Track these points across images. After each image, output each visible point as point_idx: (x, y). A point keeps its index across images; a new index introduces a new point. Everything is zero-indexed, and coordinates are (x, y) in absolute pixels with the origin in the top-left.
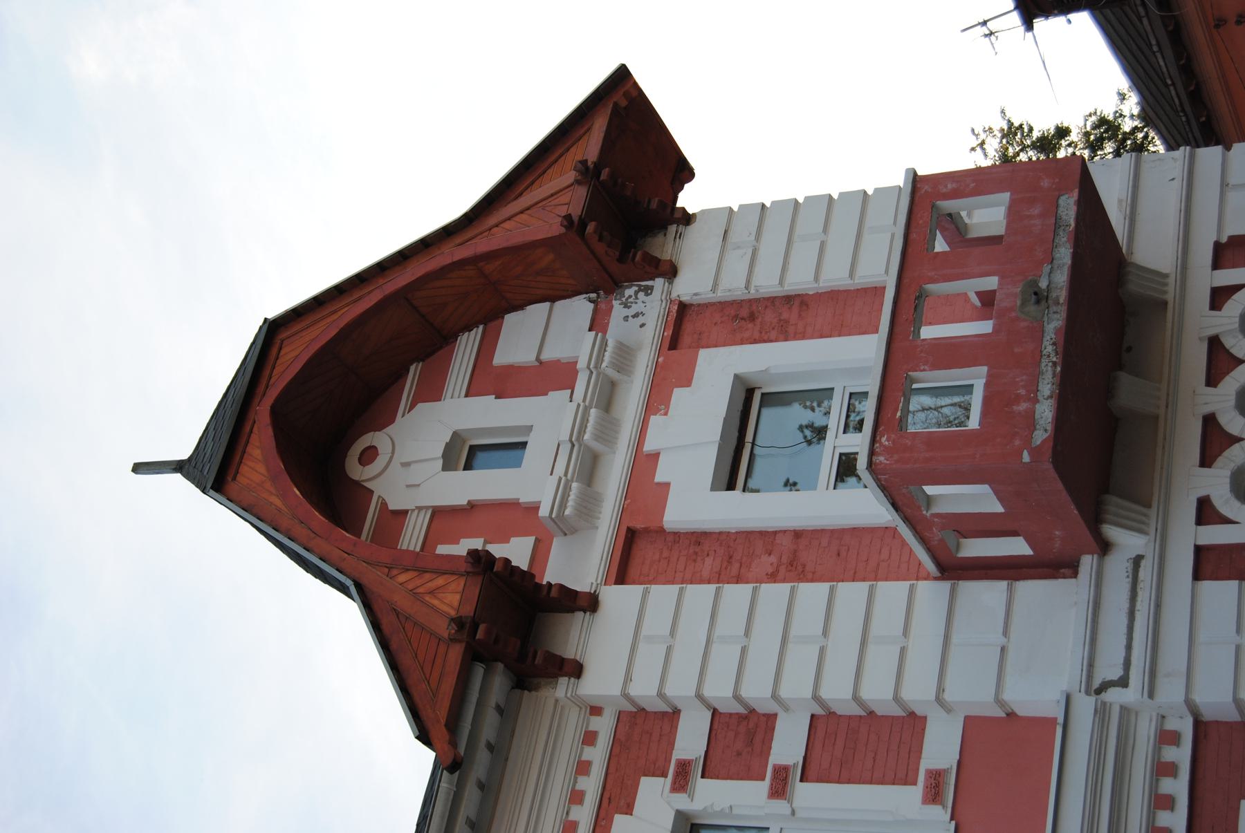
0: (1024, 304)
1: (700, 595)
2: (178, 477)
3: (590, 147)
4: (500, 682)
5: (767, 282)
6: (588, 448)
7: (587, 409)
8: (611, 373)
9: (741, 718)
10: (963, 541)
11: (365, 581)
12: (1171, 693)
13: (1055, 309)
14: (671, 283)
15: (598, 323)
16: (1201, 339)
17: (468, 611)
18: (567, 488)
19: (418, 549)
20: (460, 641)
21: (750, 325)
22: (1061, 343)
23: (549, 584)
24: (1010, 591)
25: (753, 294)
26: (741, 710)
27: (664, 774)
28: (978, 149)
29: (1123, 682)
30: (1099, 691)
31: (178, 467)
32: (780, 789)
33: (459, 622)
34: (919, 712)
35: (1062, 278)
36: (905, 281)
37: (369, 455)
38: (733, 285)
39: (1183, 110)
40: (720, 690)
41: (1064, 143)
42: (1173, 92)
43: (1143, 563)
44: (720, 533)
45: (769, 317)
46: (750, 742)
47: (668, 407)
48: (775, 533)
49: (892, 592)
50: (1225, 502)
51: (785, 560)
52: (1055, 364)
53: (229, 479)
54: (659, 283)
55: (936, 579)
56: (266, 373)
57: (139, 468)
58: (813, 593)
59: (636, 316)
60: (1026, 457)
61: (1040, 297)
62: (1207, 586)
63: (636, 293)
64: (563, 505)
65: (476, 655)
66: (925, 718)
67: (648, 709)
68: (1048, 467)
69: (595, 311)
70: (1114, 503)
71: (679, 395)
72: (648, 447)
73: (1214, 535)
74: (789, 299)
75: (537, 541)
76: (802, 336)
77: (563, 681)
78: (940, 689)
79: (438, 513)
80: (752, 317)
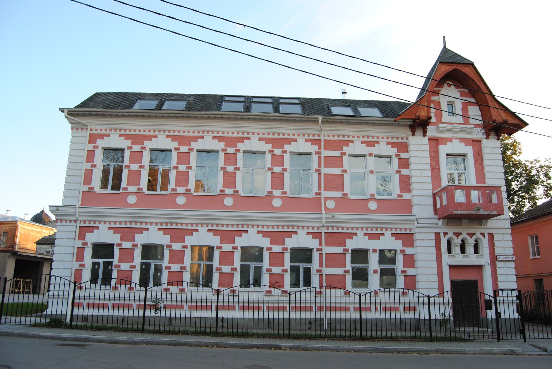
0: (477, 207)
1: (428, 154)
2: (443, 46)
3: (511, 121)
4: (410, 123)
5: (485, 156)
6: (452, 129)
7: (460, 128)
8: (467, 131)
9: (408, 163)
10: (439, 197)
11: (425, 97)
12: (417, 230)
13: (476, 212)
14: (485, 139)
15: (476, 126)
16: (475, 232)
17: (421, 118)
18: (445, 128)
19: (431, 100)
20: (416, 117)
21: (477, 154)
22: (471, 214)
23: (427, 129)
24: (431, 205)
25: (483, 154)
26: (409, 164)
27: (398, 152)
28: (546, 160)
29: (418, 223)
30: (416, 220)
31: (445, 47)
32: (398, 172)
33: (419, 117)
34: (411, 192)
35: (482, 213)
36: (481, 187)
37: (449, 85)
38: (485, 150)
39: (542, 212)
40: (412, 160)
41: (547, 179)
42: (546, 210)
43: (437, 225)
44: (438, 155)
45: (479, 157)
46: (404, 165)
47: (461, 142)
48: (439, 165)
49: (430, 186)
50: (447, 237)
51: (434, 167)
52: (467, 213)
53: (442, 64)
54: (485, 136)
55: (433, 193)
56: (463, 65)
57: (444, 37)
58: (429, 173)
59: (478, 133)
60: (451, 210)
61: (478, 210)
62: (434, 235)
63: (483, 132)
64: (441, 128)
65: (414, 120)
66: (410, 193)
67: (408, 148)
68: (449, 213)
69: (479, 124)
70: (446, 221)
71: (463, 144)
72: (453, 140)
73: (442, 235)
74: (482, 161)
75: (435, 122)
76: (475, 164)
77: (411, 133)
78: (415, 196)
79: (439, 102)
80: (479, 154)
